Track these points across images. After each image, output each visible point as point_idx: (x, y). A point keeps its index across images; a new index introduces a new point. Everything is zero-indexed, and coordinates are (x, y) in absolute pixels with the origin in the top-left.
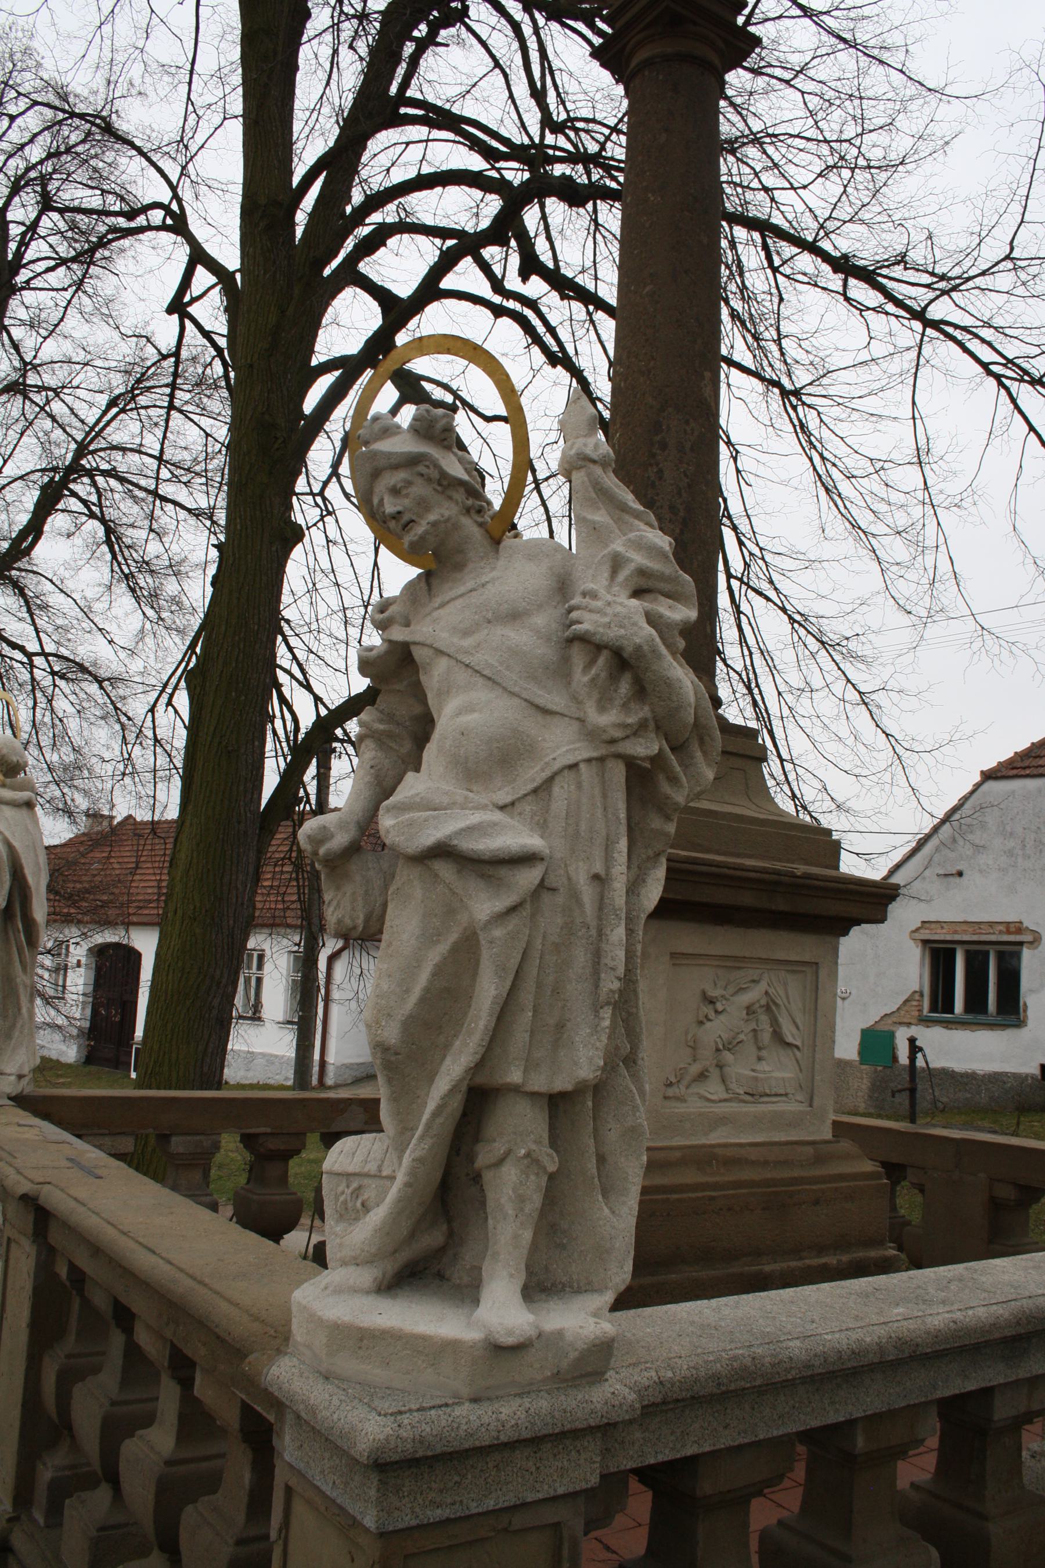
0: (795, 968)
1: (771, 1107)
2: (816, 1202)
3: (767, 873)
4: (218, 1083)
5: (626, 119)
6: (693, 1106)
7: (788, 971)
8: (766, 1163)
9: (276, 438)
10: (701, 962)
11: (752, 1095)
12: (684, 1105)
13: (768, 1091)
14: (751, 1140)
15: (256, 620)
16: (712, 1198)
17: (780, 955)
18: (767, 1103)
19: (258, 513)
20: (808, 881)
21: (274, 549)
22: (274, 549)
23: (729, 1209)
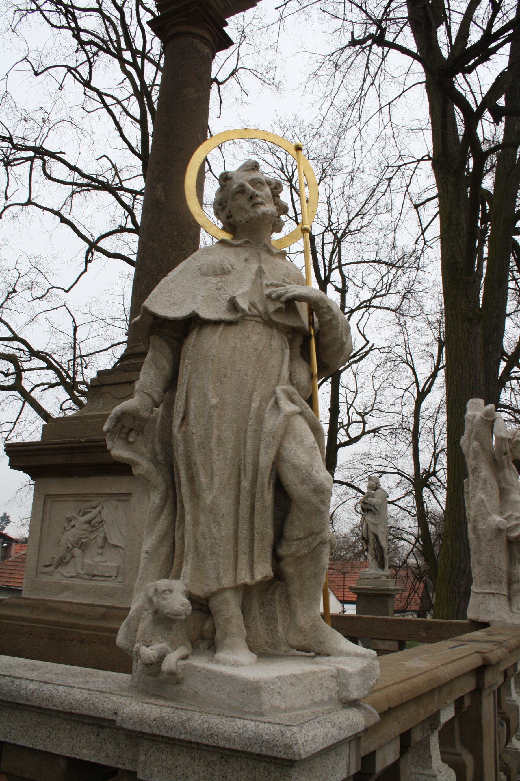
0: (121, 498)
1: (99, 583)
2: (82, 642)
3: (65, 443)
4: (465, 617)
5: (149, 89)
6: (56, 578)
7: (119, 500)
8: (69, 613)
9: (458, 269)
10: (66, 499)
11: (88, 575)
12: (50, 577)
13: (97, 574)
14: (82, 601)
15: (460, 367)
16: (23, 626)
17: (107, 491)
18: (98, 581)
19: (454, 311)
20: (88, 444)
21: (465, 327)
22: (465, 327)
23: (31, 634)
